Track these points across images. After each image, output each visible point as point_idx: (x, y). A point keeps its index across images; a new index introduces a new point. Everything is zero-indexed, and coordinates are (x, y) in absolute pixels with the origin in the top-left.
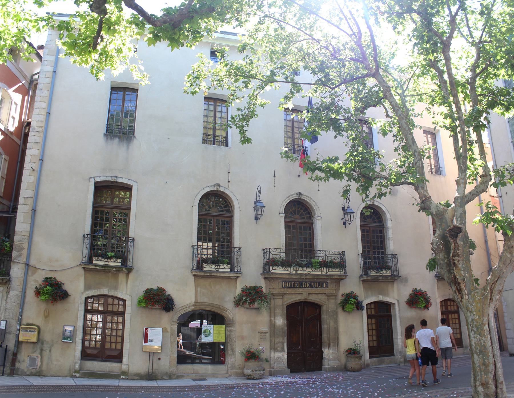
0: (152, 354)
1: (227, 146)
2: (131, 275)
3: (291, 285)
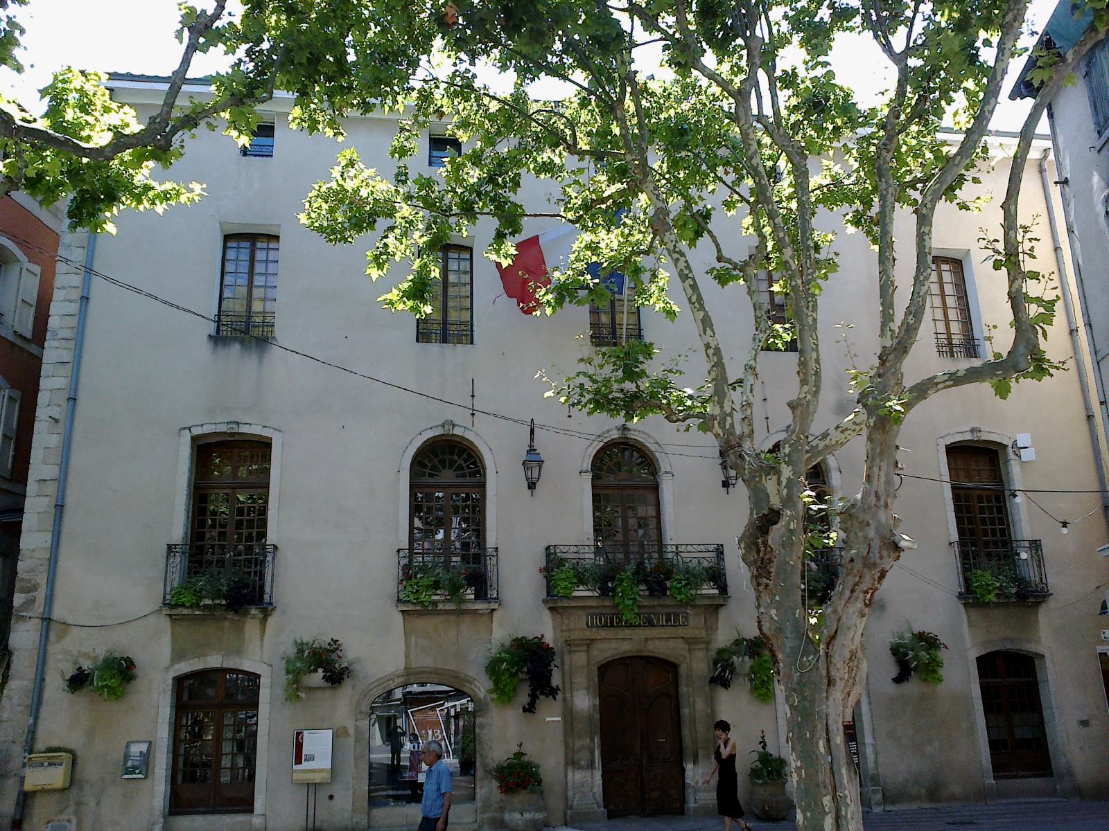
0: (312, 788)
1: (472, 343)
2: (271, 621)
3: (606, 622)
